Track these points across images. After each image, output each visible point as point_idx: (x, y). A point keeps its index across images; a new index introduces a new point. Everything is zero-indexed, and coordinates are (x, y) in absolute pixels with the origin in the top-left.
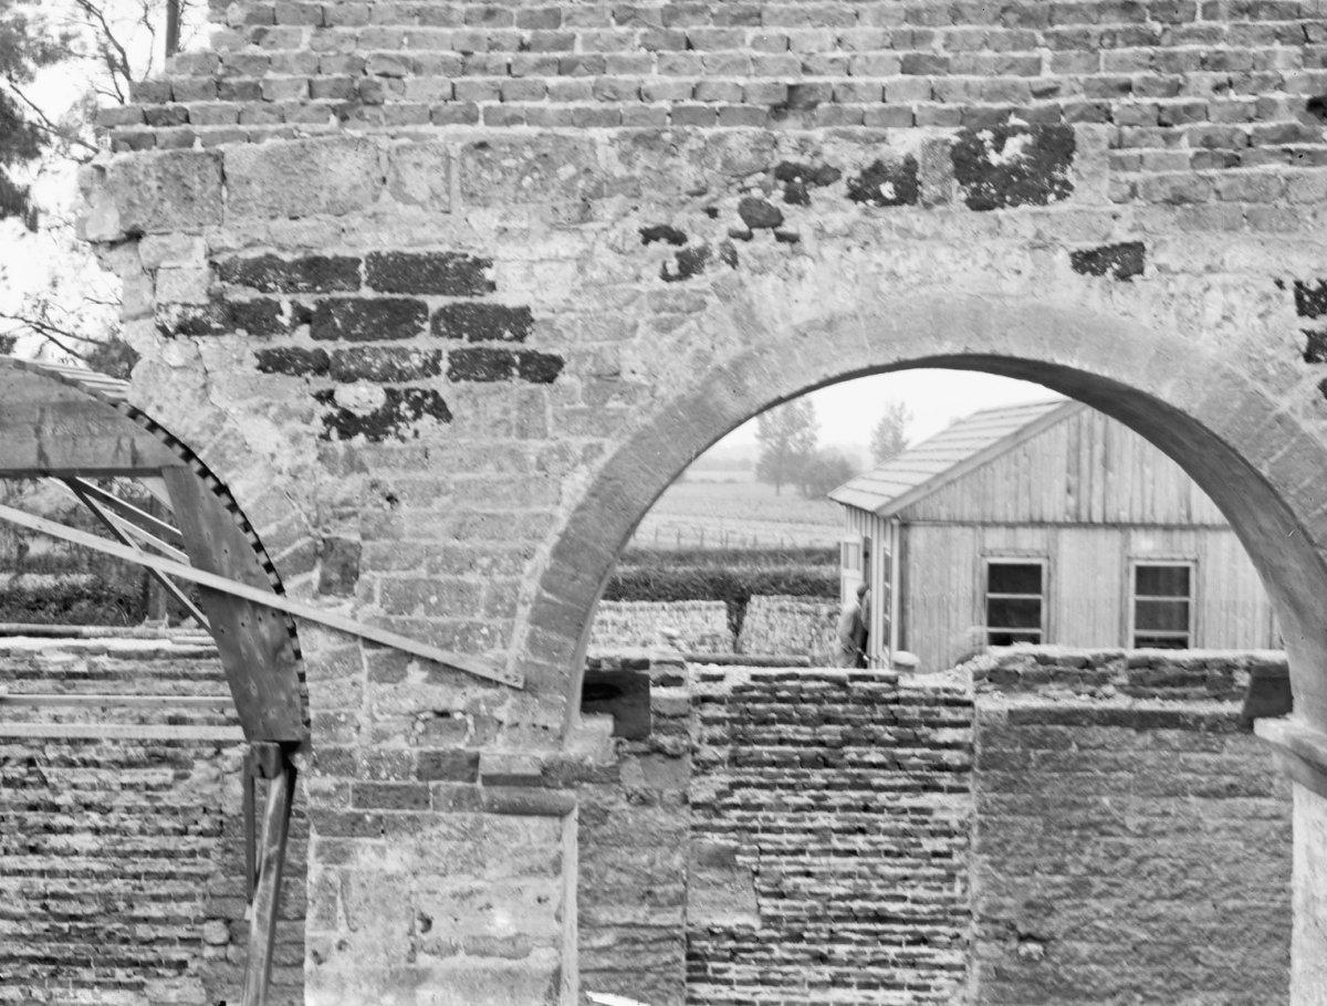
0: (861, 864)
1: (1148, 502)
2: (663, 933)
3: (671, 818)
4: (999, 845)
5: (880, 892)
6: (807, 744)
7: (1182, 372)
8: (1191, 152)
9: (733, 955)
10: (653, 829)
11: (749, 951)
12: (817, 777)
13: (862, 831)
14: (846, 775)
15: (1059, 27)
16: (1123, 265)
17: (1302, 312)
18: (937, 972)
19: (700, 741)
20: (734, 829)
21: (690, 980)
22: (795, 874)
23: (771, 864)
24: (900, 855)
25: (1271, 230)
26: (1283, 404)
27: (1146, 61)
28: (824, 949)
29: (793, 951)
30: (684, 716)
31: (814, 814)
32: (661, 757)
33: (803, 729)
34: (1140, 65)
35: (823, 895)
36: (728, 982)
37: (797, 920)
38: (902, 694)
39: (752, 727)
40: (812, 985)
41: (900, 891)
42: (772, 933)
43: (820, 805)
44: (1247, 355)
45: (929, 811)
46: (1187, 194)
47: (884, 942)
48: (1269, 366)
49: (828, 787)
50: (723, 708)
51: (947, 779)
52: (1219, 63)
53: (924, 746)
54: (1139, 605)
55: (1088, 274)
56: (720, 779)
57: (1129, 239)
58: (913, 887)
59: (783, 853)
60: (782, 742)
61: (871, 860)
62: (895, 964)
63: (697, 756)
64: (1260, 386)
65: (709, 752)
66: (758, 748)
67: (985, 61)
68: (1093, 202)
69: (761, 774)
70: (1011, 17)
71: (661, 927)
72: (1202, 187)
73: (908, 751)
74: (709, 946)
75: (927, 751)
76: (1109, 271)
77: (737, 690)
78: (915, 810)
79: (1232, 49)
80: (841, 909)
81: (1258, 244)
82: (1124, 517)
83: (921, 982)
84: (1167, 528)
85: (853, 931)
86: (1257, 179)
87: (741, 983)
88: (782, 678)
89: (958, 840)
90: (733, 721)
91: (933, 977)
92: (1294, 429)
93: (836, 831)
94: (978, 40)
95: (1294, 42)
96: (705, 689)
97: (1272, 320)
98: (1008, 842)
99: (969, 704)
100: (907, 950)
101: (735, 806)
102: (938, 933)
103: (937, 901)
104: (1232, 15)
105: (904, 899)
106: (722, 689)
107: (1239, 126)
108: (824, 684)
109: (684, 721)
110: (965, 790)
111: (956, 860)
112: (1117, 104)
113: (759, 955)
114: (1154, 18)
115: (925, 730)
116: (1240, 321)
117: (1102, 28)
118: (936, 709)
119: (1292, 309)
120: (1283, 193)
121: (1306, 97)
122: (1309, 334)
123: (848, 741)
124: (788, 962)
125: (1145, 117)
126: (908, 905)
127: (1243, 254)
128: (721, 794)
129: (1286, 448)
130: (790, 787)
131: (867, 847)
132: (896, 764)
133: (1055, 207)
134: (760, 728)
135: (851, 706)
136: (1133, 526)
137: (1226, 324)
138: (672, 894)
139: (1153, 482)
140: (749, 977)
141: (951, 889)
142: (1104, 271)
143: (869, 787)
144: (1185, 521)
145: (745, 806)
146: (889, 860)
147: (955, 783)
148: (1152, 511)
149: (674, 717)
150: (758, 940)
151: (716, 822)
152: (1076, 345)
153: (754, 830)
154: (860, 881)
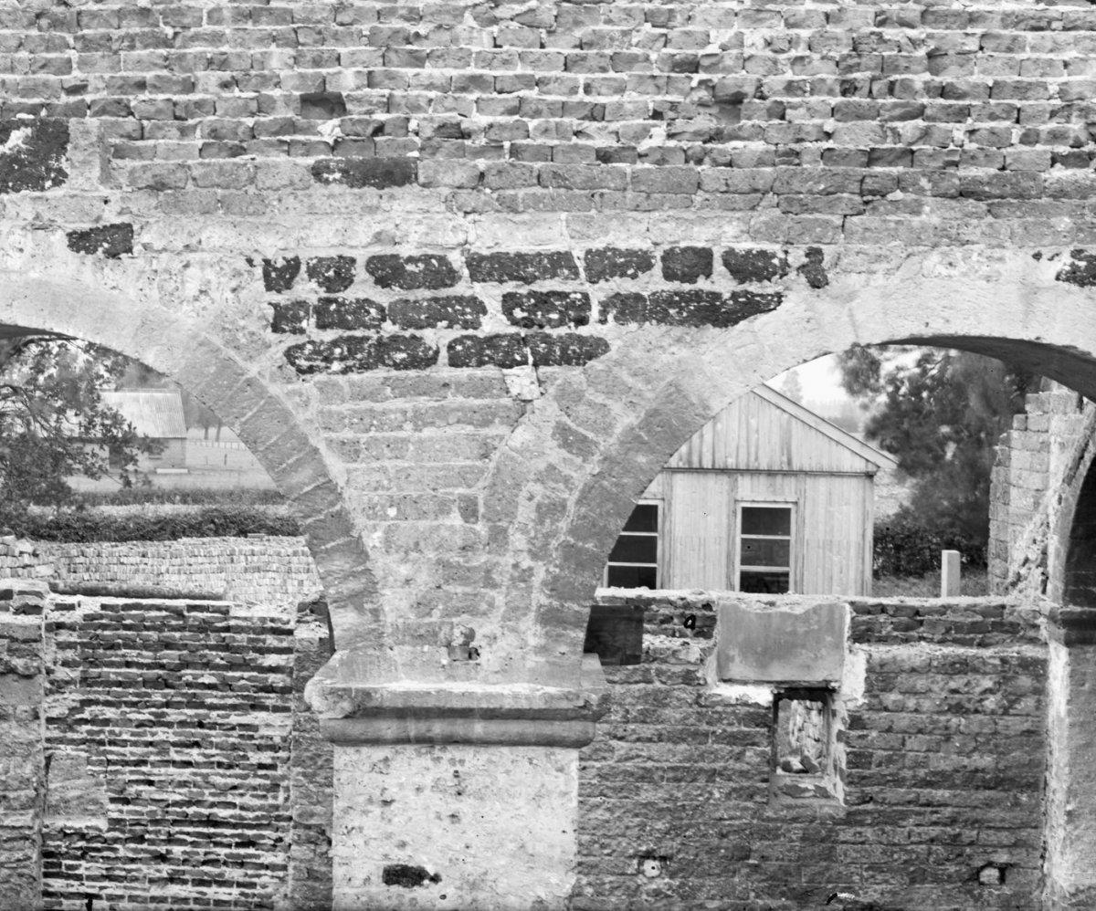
0: (195, 774)
1: (753, 450)
2: (15, 834)
3: (23, 731)
4: (311, 759)
5: (211, 799)
6: (149, 666)
7: (164, 340)
8: (199, 143)
9: (84, 855)
10: (8, 741)
11: (98, 850)
12: (157, 697)
13: (197, 744)
14: (184, 695)
15: (86, 31)
16: (111, 243)
17: (269, 288)
18: (263, 872)
19: (55, 663)
20: (84, 742)
21: (46, 875)
22: (137, 782)
23: (116, 772)
24: (230, 767)
25: (242, 214)
26: (253, 370)
27: (160, 62)
28: (162, 849)
29: (134, 851)
30: (35, 641)
31: (154, 730)
32: (16, 677)
33: (145, 653)
34: (155, 65)
35: (162, 800)
36: (79, 878)
37: (138, 824)
38: (232, 623)
39: (101, 651)
40: (152, 881)
41: (230, 798)
42: (117, 834)
43: (159, 722)
44: (223, 326)
45: (254, 728)
46: (166, 181)
47: (217, 844)
48: (240, 335)
49: (167, 705)
50: (75, 634)
51: (272, 700)
52: (221, 63)
53: (253, 669)
54: (744, 541)
55: (82, 253)
56: (73, 697)
57: (118, 221)
58: (242, 795)
59: (126, 763)
60: (128, 664)
61: (204, 771)
62: (225, 863)
63: (52, 677)
64: (232, 353)
65: (62, 673)
66: (105, 669)
67: (20, 61)
68: (85, 189)
69: (108, 693)
70: (44, 22)
71: (14, 828)
72: (180, 174)
73: (238, 674)
74: (63, 846)
75: (255, 674)
76: (100, 249)
77: (86, 617)
78: (242, 726)
79: (233, 51)
80: (177, 814)
81: (230, 226)
82: (731, 463)
83: (247, 879)
84: (770, 473)
85: (188, 834)
86: (228, 168)
87: (89, 878)
88: (127, 607)
89: (282, 754)
90: (83, 645)
91: (259, 876)
92: (262, 392)
93: (174, 744)
94: (14, 43)
95: (287, 45)
96: (57, 617)
97: (243, 294)
98: (319, 756)
99: (290, 632)
100: (234, 851)
101: (86, 721)
102: (263, 837)
103: (261, 808)
104: (236, 21)
105: (233, 805)
106: (75, 617)
107: (243, 120)
108: (164, 613)
109: (34, 645)
110: (287, 709)
111: (279, 772)
112: (134, 100)
113: (106, 854)
114: (166, 24)
115: (252, 655)
116: (215, 295)
117: (122, 32)
118: (263, 637)
119: (261, 285)
120: (252, 180)
121: (297, 93)
122: (276, 306)
123: (186, 665)
124: (133, 860)
125: (159, 111)
126: (237, 812)
127: (216, 234)
128: (72, 710)
129: (255, 410)
130: (134, 704)
131: (201, 759)
132: (227, 685)
133: (54, 193)
134: (108, 652)
135: (187, 634)
136: (738, 471)
137: (203, 297)
138: (23, 799)
139: (757, 431)
140: (97, 873)
141: (275, 798)
142: (95, 250)
143: (202, 705)
144: (785, 468)
145: (92, 721)
146: (221, 771)
147: (279, 703)
148: (757, 459)
149: (25, 641)
150: (105, 841)
151: (70, 735)
152: (72, 316)
153: (101, 743)
154: (195, 790)
